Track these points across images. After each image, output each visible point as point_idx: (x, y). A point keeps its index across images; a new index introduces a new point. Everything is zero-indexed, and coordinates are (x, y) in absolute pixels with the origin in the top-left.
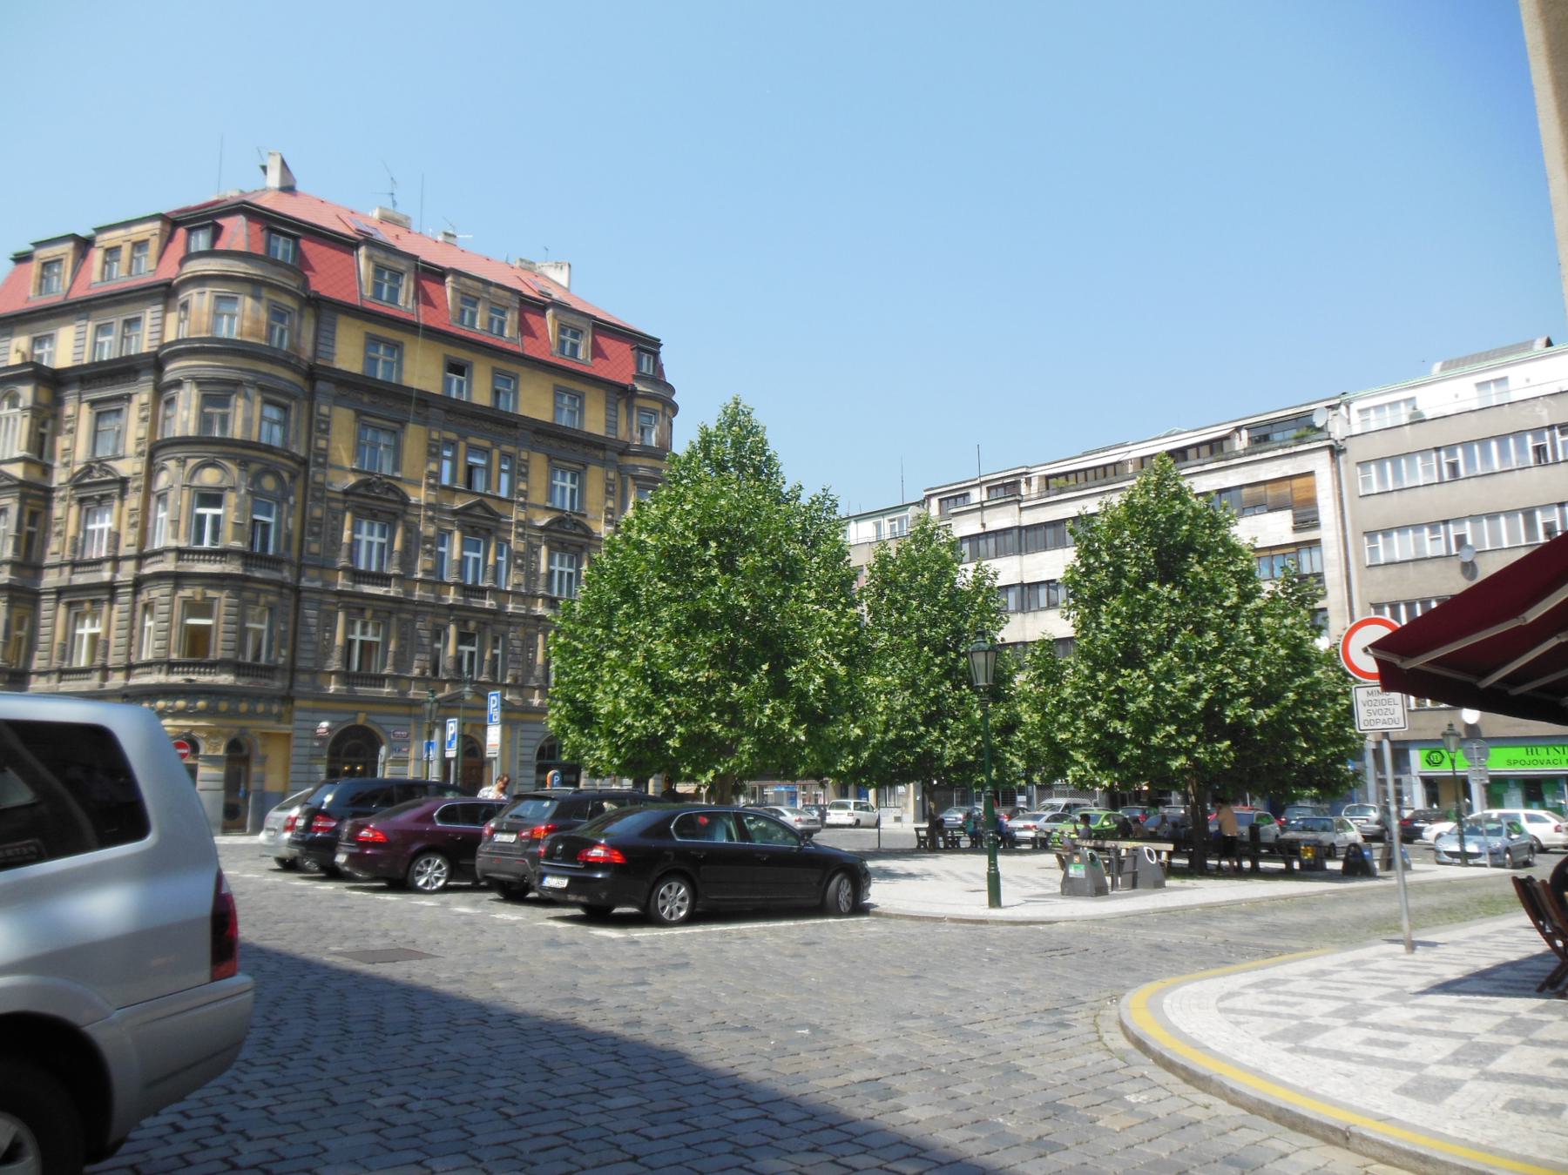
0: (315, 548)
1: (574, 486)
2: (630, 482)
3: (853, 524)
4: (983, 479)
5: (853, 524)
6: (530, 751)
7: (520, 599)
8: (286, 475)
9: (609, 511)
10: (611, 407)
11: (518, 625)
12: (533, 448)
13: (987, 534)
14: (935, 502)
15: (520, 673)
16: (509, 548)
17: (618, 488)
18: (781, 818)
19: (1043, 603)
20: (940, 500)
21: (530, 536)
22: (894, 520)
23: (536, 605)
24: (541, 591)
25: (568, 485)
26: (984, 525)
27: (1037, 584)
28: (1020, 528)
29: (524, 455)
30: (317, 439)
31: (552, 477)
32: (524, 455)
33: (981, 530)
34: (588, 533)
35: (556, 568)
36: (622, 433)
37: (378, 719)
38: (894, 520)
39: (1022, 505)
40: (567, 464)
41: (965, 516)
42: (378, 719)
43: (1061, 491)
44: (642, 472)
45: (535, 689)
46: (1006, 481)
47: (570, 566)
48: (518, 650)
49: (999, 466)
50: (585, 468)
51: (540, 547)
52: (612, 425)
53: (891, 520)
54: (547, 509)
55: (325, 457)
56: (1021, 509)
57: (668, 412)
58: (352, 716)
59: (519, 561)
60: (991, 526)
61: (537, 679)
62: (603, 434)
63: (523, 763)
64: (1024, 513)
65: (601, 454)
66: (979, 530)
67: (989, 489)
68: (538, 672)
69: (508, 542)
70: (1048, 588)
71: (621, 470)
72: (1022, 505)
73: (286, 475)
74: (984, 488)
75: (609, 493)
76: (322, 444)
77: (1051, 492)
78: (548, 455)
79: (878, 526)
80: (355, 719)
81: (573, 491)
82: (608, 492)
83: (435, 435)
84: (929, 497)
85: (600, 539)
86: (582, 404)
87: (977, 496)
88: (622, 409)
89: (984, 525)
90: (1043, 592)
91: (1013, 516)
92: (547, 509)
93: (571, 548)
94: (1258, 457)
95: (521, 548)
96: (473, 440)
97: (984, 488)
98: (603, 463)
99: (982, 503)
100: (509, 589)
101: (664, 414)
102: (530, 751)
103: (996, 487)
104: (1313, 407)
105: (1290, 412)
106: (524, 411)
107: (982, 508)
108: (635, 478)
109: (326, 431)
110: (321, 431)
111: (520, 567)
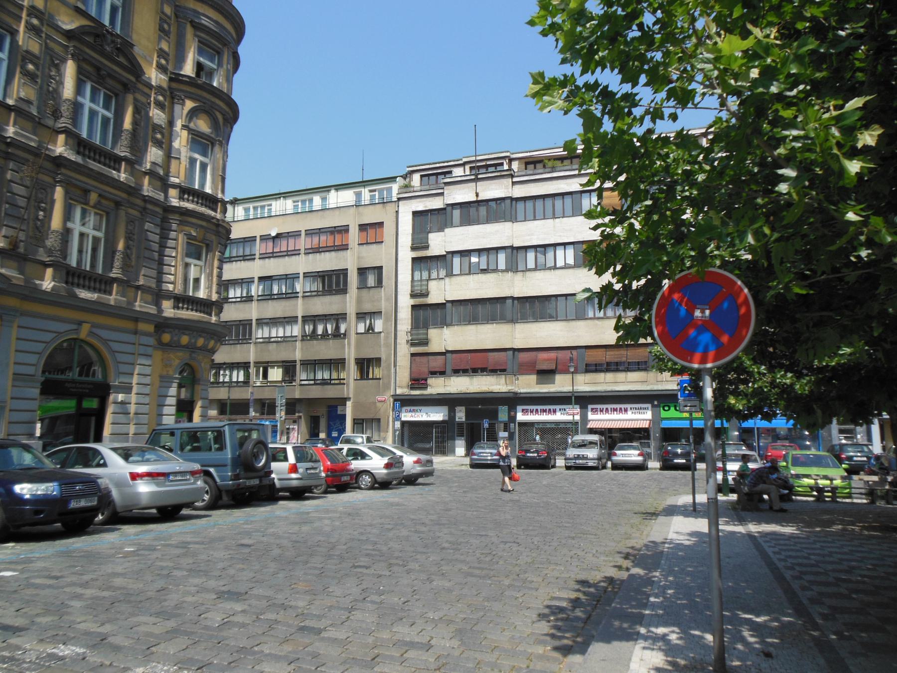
2: (189, 31)
3: (333, 192)
5: (333, 192)
6: (33, 359)
7: (29, 125)
9: (162, 54)
11: (25, 162)
13: (478, 203)
14: (416, 178)
15: (22, 236)
16: (14, 42)
17: (173, 29)
18: (405, 474)
19: (531, 264)
20: (422, 176)
21: (48, 37)
22: (374, 191)
23: (55, 143)
24: (63, 123)
26: (477, 195)
27: (526, 248)
28: (511, 199)
33: (474, 199)
34: (136, 71)
35: (86, 101)
37: (104, 334)
38: (374, 191)
39: (515, 179)
42: (104, 334)
44: (205, 21)
45: (46, 265)
46: (489, 163)
47: (107, 107)
48: (22, 202)
49: (486, 152)
51: (64, 61)
53: (371, 191)
54: (78, 10)
56: (514, 183)
58: (75, 327)
59: (31, 67)
60: (484, 196)
61: (50, 252)
63: (18, 377)
64: (517, 187)
66: (472, 198)
68: (51, 241)
69: (14, 33)
70: (536, 252)
72: (515, 179)
74: (467, 167)
75: (163, 32)
79: (359, 195)
80: (77, 331)
82: (161, 29)
85: (150, 87)
87: (458, 172)
89: (477, 195)
90: (531, 255)
91: (506, 187)
92: (78, 10)
93: (110, 82)
95: (34, 47)
97: (467, 167)
100: (10, 102)
102: (33, 359)
103: (479, 167)
108: (197, 27)
111: (31, 77)
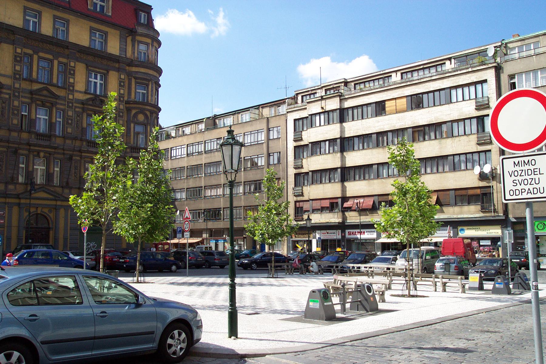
0: (69, 130)
1: (102, 82)
4: (322, 85)
8: (148, 113)
10: (123, 40)
12: (78, 60)
25: (98, 81)
29: (72, 64)
30: (69, 78)
31: (88, 76)
32: (72, 64)
36: (129, 54)
40: (98, 70)
41: (313, 104)
43: (361, 90)
46: (335, 86)
50: (108, 72)
52: (123, 49)
55: (73, 87)
57: (155, 44)
62: (118, 54)
65: (117, 65)
67: (326, 90)
71: (129, 75)
73: (148, 113)
76: (71, 80)
77: (356, 91)
78: (86, 65)
81: (101, 84)
82: (120, 85)
83: (19, 50)
84: (297, 94)
86: (106, 37)
88: (129, 39)
94: (459, 72)
96: (41, 54)
97: (324, 89)
98: (118, 70)
99: (322, 97)
101: (152, 46)
104: (487, 47)
105: (476, 50)
106: (72, 39)
107: (322, 98)
108: (136, 78)
109: (74, 74)
110: (70, 74)
